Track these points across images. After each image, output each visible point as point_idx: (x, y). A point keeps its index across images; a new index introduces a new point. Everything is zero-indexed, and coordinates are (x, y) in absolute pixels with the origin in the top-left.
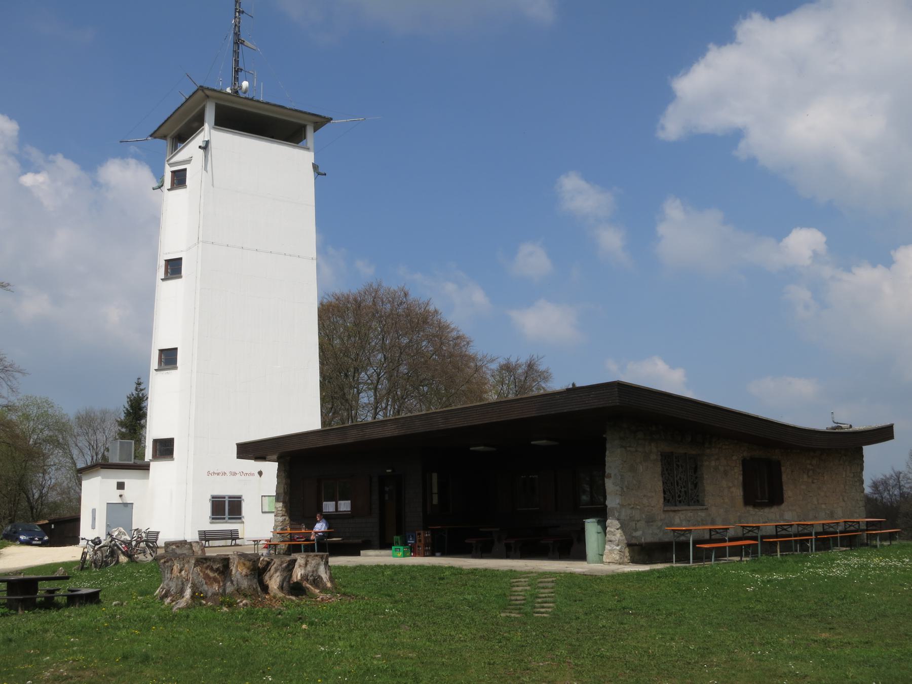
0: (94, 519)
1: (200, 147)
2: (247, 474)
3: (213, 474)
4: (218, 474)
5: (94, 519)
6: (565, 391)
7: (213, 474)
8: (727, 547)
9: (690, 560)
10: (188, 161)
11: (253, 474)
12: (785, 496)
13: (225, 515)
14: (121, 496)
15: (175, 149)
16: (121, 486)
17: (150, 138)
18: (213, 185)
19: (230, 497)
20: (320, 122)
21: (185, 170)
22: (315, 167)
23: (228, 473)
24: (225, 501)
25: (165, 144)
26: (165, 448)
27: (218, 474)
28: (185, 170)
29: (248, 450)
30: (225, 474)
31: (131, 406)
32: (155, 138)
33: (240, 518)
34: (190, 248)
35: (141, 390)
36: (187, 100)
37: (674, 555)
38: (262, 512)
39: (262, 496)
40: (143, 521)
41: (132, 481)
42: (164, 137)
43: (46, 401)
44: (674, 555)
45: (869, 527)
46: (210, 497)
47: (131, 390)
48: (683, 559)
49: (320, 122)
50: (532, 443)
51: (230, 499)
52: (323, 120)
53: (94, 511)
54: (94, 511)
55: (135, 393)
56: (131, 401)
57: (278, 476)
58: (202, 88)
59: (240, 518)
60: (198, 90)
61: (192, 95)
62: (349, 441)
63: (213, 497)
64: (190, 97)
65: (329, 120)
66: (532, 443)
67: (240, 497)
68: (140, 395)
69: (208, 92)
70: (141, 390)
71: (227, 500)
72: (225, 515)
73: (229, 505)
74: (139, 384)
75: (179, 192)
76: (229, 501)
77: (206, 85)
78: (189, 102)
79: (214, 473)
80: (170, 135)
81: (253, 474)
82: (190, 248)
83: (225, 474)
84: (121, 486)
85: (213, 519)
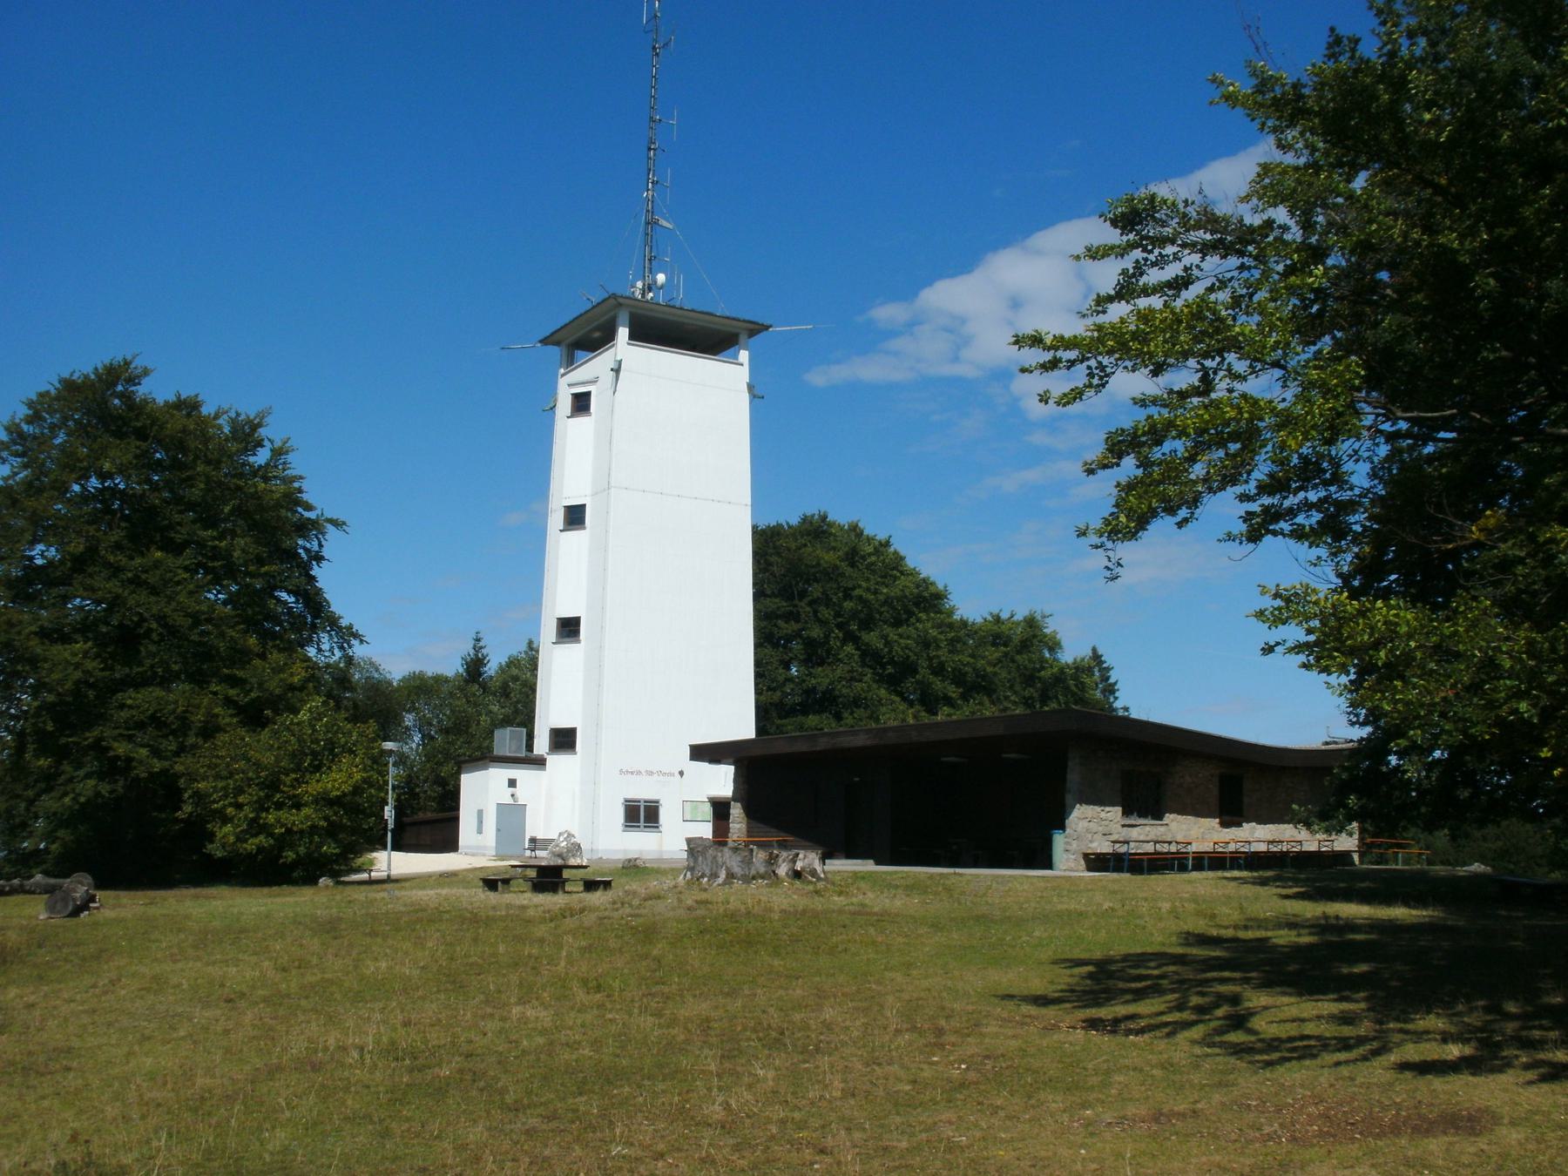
0: (480, 822)
1: (612, 370)
4: (632, 773)
5: (480, 822)
8: (1190, 867)
10: (594, 381)
11: (673, 775)
14: (513, 795)
15: (570, 362)
16: (512, 783)
17: (539, 345)
19: (645, 802)
20: (756, 329)
21: (588, 394)
22: (750, 387)
25: (555, 352)
26: (564, 740)
27: (632, 773)
28: (588, 394)
29: (702, 753)
30: (639, 773)
31: (467, 671)
32: (546, 344)
33: (657, 827)
34: (596, 493)
35: (481, 648)
36: (594, 307)
40: (538, 825)
41: (521, 774)
42: (558, 343)
43: (372, 664)
47: (467, 648)
49: (756, 329)
50: (1005, 756)
52: (757, 327)
53: (480, 813)
54: (480, 813)
55: (472, 652)
56: (467, 664)
57: (735, 781)
58: (614, 296)
59: (657, 827)
60: (610, 297)
62: (818, 749)
63: (626, 801)
64: (599, 304)
65: (767, 328)
66: (1005, 756)
67: (657, 802)
68: (480, 655)
69: (621, 300)
70: (481, 648)
73: (645, 812)
74: (478, 640)
75: (582, 421)
77: (619, 292)
78: (595, 310)
80: (567, 341)
81: (673, 775)
82: (596, 493)
83: (639, 773)
84: (512, 783)
85: (626, 826)
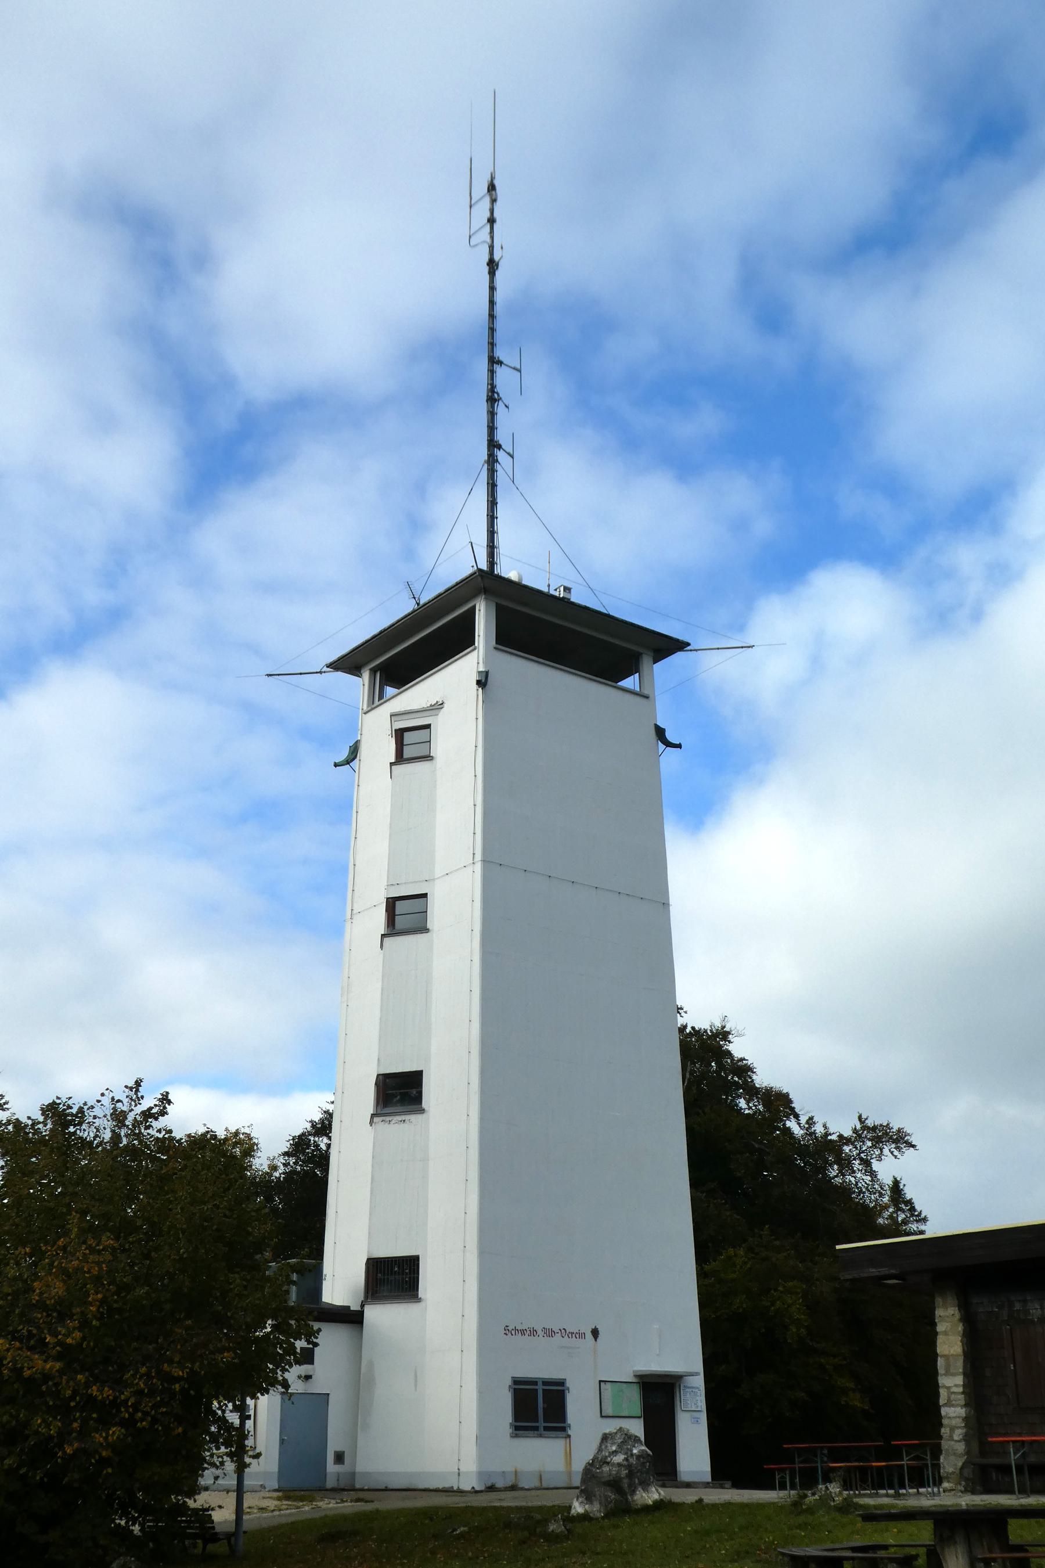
2: (572, 1333)
3: (513, 1332)
4: (523, 1332)
6: (490, 268)
7: (513, 1332)
9: (1016, 1467)
11: (581, 1335)
12: (867, 1523)
13: (537, 1421)
18: (391, 778)
23: (540, 1332)
24: (537, 1390)
30: (533, 1332)
33: (563, 1429)
37: (917, 1442)
38: (602, 1416)
39: (600, 1381)
44: (917, 1442)
45: (1013, 1447)
46: (509, 1382)
48: (306, 1257)
51: (517, 1387)
61: (403, 714)
71: (540, 1388)
72: (537, 1421)
76: (544, 1390)
79: (516, 1329)
81: (581, 1335)
83: (533, 1332)
